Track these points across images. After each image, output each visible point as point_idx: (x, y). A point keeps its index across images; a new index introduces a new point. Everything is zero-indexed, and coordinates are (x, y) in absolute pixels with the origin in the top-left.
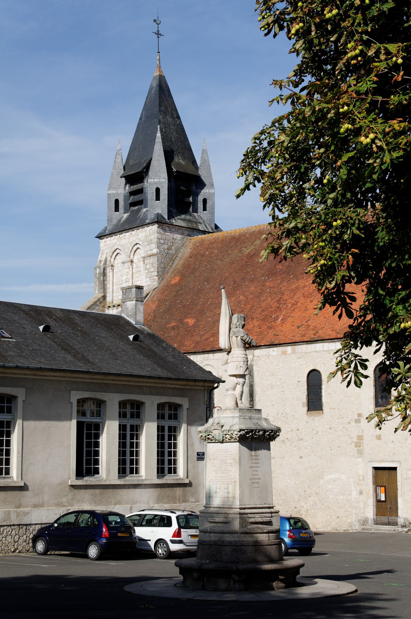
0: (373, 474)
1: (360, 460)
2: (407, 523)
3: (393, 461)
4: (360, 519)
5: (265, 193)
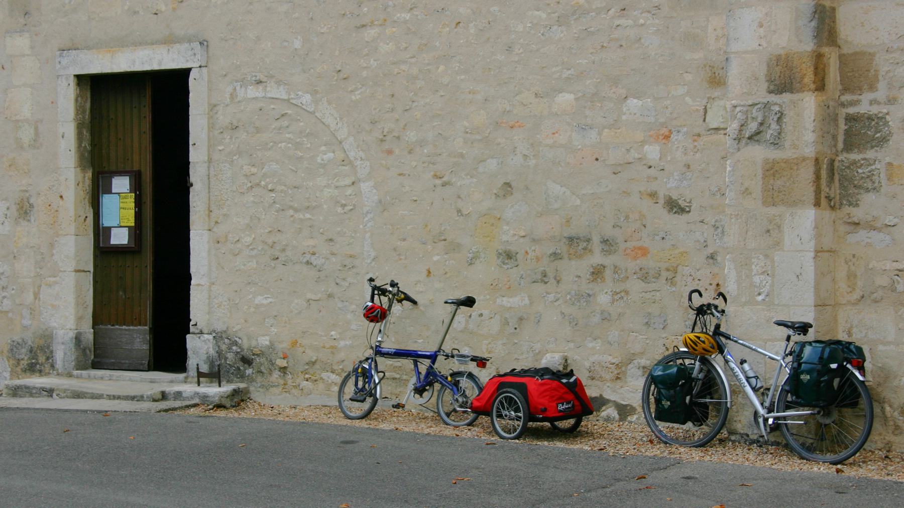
0: (79, 110)
1: (21, 43)
2: (230, 356)
3: (170, 41)
4: (17, 338)
5: (866, 481)
